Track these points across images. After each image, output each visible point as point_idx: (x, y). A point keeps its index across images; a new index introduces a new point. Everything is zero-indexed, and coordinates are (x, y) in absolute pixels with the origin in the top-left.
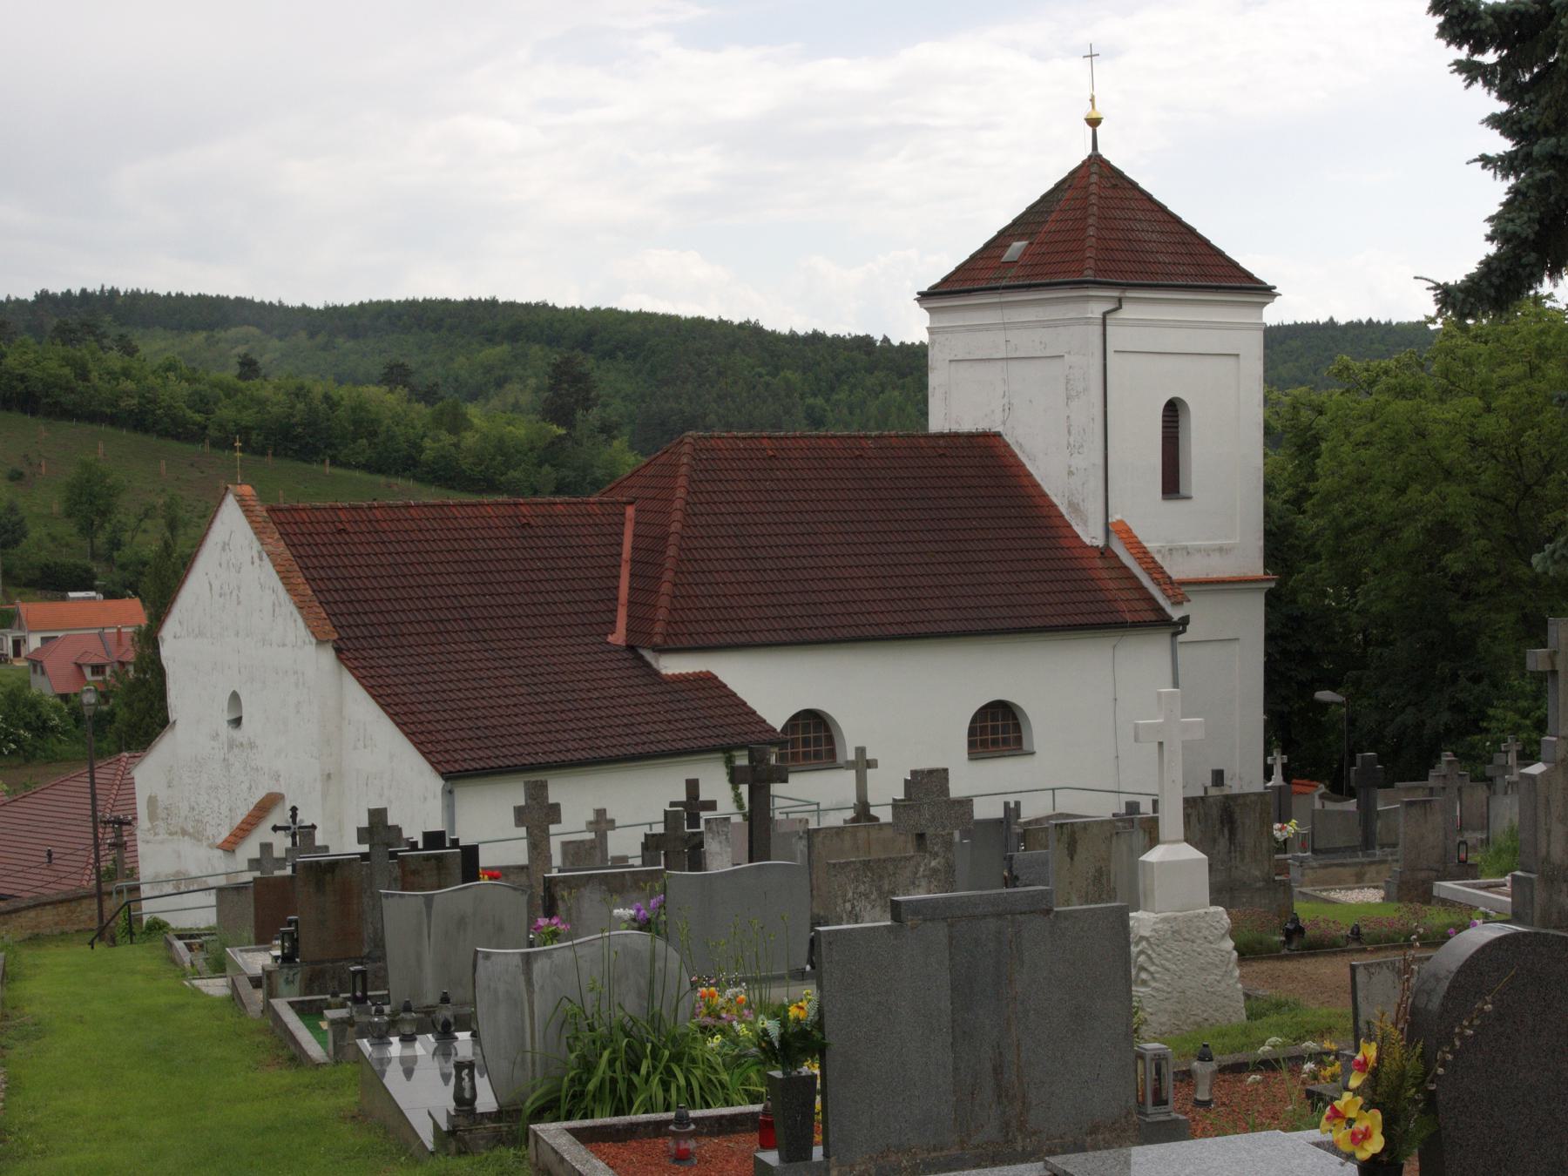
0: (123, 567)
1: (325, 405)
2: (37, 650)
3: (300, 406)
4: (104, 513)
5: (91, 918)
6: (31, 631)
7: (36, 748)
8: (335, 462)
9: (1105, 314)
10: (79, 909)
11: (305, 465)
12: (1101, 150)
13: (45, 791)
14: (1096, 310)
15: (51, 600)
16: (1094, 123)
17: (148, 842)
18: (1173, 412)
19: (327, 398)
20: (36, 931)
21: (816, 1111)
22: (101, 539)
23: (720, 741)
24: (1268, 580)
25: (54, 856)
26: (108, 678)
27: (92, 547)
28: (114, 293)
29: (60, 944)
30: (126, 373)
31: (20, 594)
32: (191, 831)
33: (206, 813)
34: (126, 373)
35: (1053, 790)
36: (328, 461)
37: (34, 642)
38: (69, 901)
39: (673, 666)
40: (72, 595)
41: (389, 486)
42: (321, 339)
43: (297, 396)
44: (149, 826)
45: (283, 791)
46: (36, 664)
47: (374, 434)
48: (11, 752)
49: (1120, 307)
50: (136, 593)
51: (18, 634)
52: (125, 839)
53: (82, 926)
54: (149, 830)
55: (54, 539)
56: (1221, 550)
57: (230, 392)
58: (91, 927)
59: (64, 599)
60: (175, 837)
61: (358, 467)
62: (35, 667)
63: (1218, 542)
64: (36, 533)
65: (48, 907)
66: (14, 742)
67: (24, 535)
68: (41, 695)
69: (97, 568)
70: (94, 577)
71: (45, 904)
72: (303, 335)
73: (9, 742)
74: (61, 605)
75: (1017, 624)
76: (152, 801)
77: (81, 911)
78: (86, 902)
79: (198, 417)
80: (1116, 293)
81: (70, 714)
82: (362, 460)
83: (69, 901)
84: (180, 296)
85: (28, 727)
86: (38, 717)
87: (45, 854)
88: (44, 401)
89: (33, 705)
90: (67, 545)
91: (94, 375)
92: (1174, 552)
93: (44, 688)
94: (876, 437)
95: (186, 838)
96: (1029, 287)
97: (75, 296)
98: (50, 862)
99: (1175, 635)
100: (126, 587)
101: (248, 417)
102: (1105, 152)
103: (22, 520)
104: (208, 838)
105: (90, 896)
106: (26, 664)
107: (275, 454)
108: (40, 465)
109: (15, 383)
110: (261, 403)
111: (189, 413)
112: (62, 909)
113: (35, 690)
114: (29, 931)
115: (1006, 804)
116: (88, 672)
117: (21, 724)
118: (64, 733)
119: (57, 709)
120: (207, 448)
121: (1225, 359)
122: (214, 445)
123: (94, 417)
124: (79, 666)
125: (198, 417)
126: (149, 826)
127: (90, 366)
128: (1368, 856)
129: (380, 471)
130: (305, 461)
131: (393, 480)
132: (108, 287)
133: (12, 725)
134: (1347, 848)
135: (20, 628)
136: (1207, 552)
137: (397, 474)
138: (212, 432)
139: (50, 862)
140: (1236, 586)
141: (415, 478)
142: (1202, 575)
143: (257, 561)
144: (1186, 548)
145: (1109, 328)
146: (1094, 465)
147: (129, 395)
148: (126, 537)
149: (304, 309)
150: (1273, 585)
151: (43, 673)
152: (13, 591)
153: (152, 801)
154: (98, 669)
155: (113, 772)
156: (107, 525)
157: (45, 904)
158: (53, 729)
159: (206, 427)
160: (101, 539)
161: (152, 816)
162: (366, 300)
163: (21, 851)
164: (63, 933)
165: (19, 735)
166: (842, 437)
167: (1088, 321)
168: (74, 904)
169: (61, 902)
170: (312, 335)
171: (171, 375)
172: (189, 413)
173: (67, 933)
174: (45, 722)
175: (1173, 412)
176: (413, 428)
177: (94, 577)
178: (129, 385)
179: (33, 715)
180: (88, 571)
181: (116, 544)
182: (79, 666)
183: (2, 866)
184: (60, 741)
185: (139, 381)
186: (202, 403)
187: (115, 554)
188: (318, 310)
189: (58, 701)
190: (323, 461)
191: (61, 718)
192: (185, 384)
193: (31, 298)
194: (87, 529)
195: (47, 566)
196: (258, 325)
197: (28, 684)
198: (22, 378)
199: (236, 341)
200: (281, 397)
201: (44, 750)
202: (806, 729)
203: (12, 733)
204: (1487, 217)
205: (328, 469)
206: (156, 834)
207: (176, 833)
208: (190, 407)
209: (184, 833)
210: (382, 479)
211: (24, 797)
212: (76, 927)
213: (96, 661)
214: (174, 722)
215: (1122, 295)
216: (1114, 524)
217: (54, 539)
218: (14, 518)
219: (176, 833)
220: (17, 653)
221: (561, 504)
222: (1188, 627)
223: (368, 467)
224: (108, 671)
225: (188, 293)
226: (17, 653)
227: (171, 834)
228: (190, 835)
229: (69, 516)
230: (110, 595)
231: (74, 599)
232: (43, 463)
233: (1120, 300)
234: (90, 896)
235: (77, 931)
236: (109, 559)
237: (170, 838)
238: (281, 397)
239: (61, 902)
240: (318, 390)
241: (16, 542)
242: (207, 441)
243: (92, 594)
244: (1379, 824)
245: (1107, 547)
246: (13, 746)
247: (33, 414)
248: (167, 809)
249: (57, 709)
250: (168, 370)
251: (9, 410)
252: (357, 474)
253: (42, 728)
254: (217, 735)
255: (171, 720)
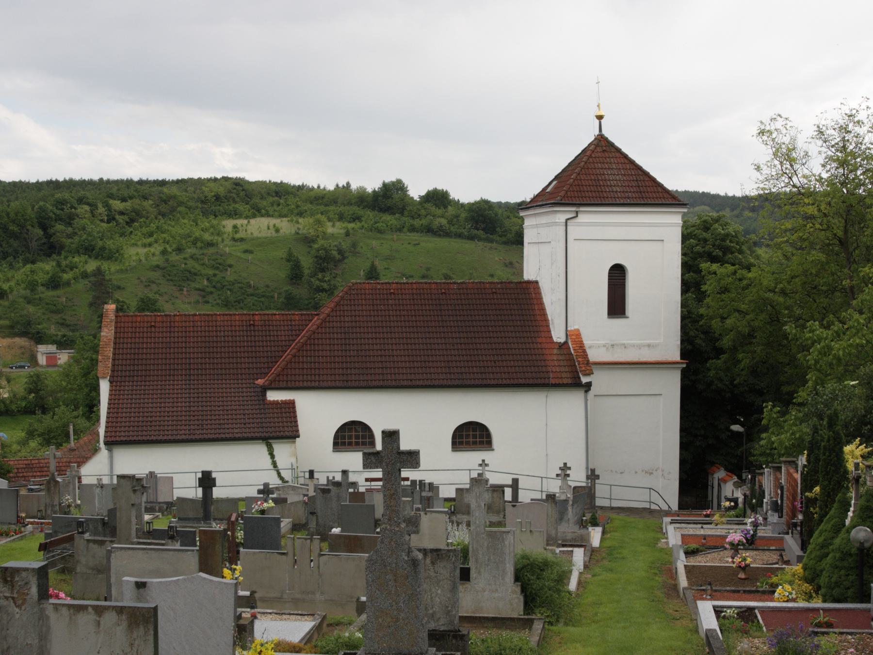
9: (567, 220)
12: (604, 132)
14: (561, 218)
16: (600, 118)
18: (618, 274)
23: (263, 435)
24: (682, 363)
35: (470, 470)
39: (273, 396)
42: (736, 212)
49: (577, 216)
56: (649, 346)
63: (648, 342)
72: (728, 209)
75: (429, 383)
80: (574, 209)
92: (615, 347)
94: (461, 283)
96: (541, 206)
97: (369, 194)
99: (586, 392)
102: (606, 133)
115: (328, 477)
121: (655, 243)
128: (207, 524)
134: (196, 518)
136: (640, 347)
140: (632, 366)
142: (635, 359)
144: (624, 344)
145: (568, 227)
146: (559, 299)
150: (684, 366)
166: (440, 283)
167: (556, 224)
170: (732, 210)
175: (618, 274)
188: (739, 198)
196: (709, 205)
202: (350, 430)
204: (350, 182)
215: (578, 210)
216: (571, 331)
221: (238, 315)
222: (592, 388)
233: (577, 212)
244: (212, 508)
245: (566, 343)
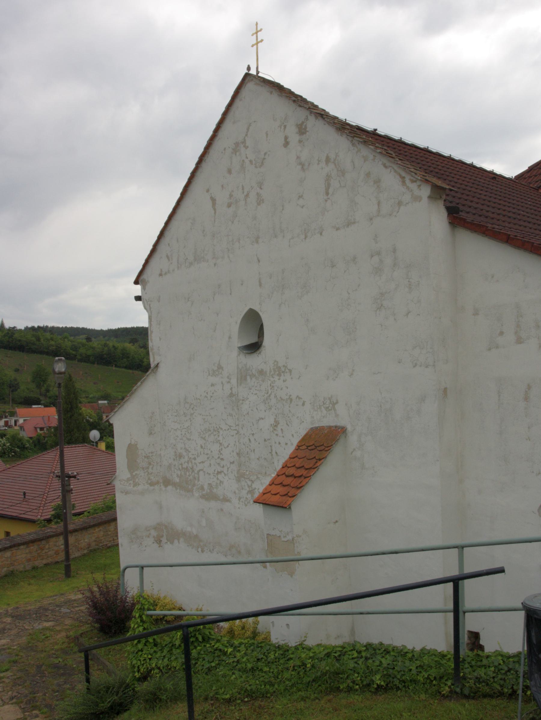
0: (50, 398)
1: (113, 349)
2: (22, 423)
3: (106, 349)
4: (44, 381)
5: (57, 553)
6: (20, 418)
7: (21, 454)
8: (116, 366)
10: (47, 546)
11: (106, 367)
13: (23, 464)
15: (27, 408)
17: (127, 493)
19: (114, 346)
20: (11, 568)
21: (479, 651)
22: (43, 389)
25: (27, 494)
26: (45, 431)
27: (40, 392)
28: (47, 327)
29: (32, 581)
30: (52, 339)
31: (17, 406)
32: (177, 480)
33: (199, 460)
34: (52, 339)
36: (114, 366)
37: (21, 421)
38: (40, 540)
40: (33, 406)
41: (133, 373)
43: (105, 346)
44: (129, 476)
45: (341, 423)
46: (21, 427)
47: (128, 357)
48: (13, 456)
50: (54, 406)
51: (16, 418)
52: (72, 487)
53: (50, 560)
54: (128, 480)
55: (28, 389)
57: (83, 345)
58: (57, 560)
59: (31, 407)
60: (156, 487)
61: (123, 367)
62: (21, 429)
64: (22, 387)
65: (22, 547)
66: (14, 452)
67: (19, 388)
68: (23, 437)
69: (42, 398)
70: (41, 401)
71: (19, 545)
72: (101, 337)
73: (12, 452)
74: (30, 409)
76: (132, 449)
77: (49, 548)
78: (53, 541)
79: (74, 353)
81: (32, 443)
82: (125, 365)
83: (40, 540)
84: (66, 327)
85: (18, 447)
86: (22, 444)
87: (22, 494)
88: (26, 348)
89: (20, 440)
90: (32, 391)
91: (42, 340)
93: (25, 435)
95: (170, 487)
98: (25, 497)
100: (51, 404)
101: (89, 353)
103: (18, 383)
104: (202, 488)
105: (61, 534)
106: (18, 428)
107: (98, 364)
108: (24, 367)
109: (17, 342)
110: (94, 348)
111: (71, 351)
112: (34, 547)
113: (21, 435)
114: (5, 569)
116: (38, 430)
117: (16, 446)
118: (31, 449)
119: (28, 441)
120: (76, 362)
122: (78, 361)
123: (41, 353)
124: (36, 428)
125: (74, 353)
126: (129, 476)
127: (41, 337)
129: (130, 369)
130: (107, 366)
131: (134, 371)
132: (45, 325)
133: (13, 447)
135: (17, 416)
137: (135, 369)
138: (78, 357)
139: (25, 497)
141: (141, 371)
143: (294, 138)
147: (53, 346)
148: (51, 389)
149: (102, 330)
151: (24, 430)
152: (15, 405)
153: (132, 449)
154: (42, 429)
155: (55, 454)
156: (45, 385)
157: (19, 545)
158: (27, 448)
159: (76, 356)
160: (43, 389)
161: (132, 465)
162: (120, 327)
163: (44, 466)
164: (34, 568)
165: (15, 450)
168: (43, 542)
169: (33, 541)
170: (104, 337)
171: (66, 340)
172: (71, 351)
173: (37, 568)
174: (24, 446)
176: (140, 355)
177: (41, 401)
178: (52, 343)
179: (20, 443)
180: (39, 399)
181: (48, 391)
182: (36, 428)
183: (2, 499)
184: (29, 452)
185: (56, 342)
186: (75, 348)
187: (48, 394)
189: (28, 439)
190: (113, 366)
191: (30, 444)
192: (70, 342)
193: (23, 328)
194: (39, 386)
195: (26, 397)
197: (19, 434)
198: (20, 341)
199: (82, 339)
200: (100, 346)
201: (23, 455)
203: (13, 450)
205: (114, 368)
206: (136, 484)
207: (158, 483)
208: (71, 349)
209: (167, 482)
210: (130, 371)
211: (13, 467)
212: (45, 562)
213: (41, 426)
214: (157, 366)
217: (28, 389)
218: (16, 383)
219: (158, 483)
220: (16, 425)
223: (126, 368)
224: (45, 429)
225: (68, 326)
226: (16, 425)
227: (152, 484)
228: (174, 485)
229: (33, 382)
230: (46, 406)
231: (34, 408)
232: (25, 366)
234: (61, 534)
235: (46, 565)
236: (45, 396)
237: (152, 488)
238: (100, 346)
239: (33, 541)
240: (111, 344)
241: (16, 390)
242: (76, 360)
243: (40, 406)
246: (13, 454)
247: (23, 352)
248: (147, 457)
249: (28, 441)
250: (65, 338)
251: (16, 351)
252: (123, 370)
253: (23, 448)
254: (220, 367)
255: (152, 365)
